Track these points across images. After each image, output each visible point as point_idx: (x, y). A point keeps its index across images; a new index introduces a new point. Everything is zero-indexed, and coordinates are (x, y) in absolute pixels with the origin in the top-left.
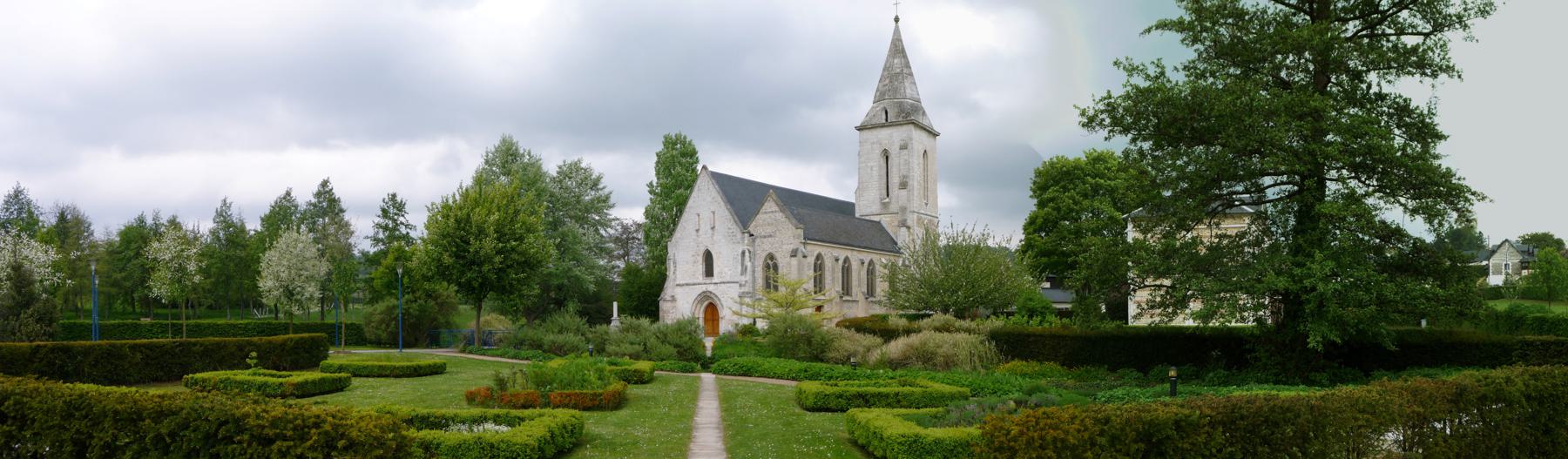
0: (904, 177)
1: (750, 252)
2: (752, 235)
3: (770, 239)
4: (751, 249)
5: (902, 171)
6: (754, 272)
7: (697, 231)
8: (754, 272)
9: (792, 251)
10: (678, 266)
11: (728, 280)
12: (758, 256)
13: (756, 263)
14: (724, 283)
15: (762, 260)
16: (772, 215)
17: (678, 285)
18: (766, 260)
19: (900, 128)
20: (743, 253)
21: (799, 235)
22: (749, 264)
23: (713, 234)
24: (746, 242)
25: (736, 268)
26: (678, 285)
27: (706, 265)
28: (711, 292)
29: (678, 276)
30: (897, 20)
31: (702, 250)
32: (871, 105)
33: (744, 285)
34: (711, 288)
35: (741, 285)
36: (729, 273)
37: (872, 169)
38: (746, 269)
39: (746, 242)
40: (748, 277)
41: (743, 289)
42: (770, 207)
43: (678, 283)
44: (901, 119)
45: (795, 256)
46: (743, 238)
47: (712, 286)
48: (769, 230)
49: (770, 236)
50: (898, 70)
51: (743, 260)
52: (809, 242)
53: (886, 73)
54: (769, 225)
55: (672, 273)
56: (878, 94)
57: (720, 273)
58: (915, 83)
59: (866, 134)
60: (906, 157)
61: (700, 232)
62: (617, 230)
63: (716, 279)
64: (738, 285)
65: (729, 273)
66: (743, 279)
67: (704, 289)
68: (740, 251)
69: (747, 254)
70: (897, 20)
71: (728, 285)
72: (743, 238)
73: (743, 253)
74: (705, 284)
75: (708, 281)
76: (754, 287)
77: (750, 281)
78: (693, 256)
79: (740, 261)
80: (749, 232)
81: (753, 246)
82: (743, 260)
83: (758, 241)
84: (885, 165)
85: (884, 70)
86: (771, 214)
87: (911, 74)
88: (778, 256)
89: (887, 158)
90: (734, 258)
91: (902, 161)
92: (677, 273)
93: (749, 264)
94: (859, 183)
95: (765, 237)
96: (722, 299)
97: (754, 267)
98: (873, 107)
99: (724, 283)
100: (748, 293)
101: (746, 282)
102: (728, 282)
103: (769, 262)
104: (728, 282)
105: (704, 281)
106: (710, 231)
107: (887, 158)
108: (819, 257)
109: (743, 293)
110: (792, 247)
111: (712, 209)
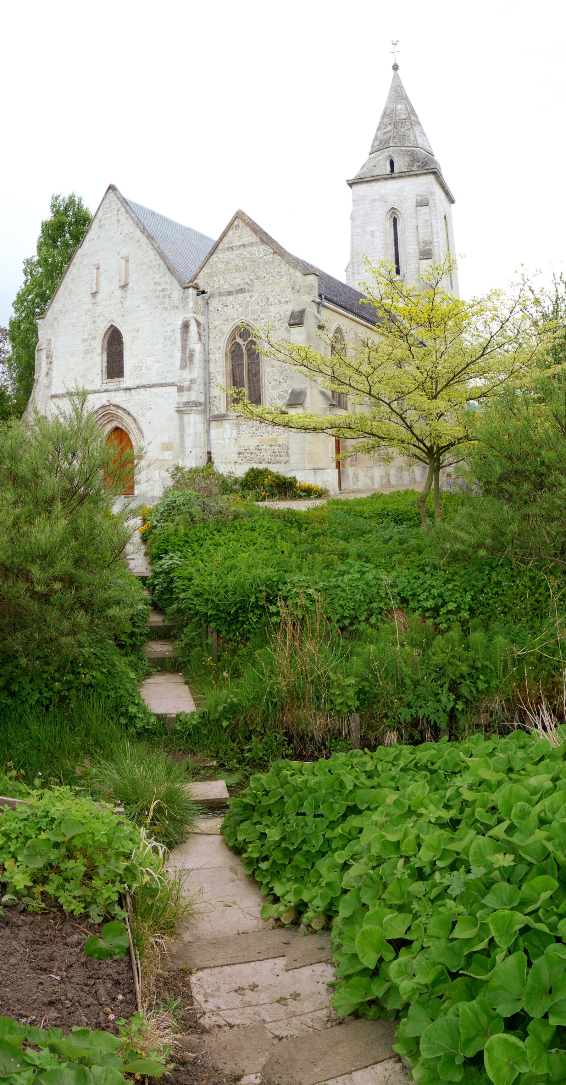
0: (425, 243)
1: (198, 324)
2: (203, 292)
3: (240, 297)
4: (202, 319)
5: (421, 236)
6: (207, 362)
7: (94, 294)
8: (207, 362)
9: (292, 315)
10: (55, 362)
11: (154, 381)
12: (214, 332)
13: (212, 345)
14: (144, 387)
15: (226, 337)
16: (245, 253)
17: (53, 397)
18: (232, 338)
19: (414, 180)
20: (186, 326)
21: (311, 287)
22: (197, 347)
23: (124, 298)
24: (191, 305)
25: (170, 357)
26: (53, 397)
27: (109, 356)
28: (117, 407)
29: (54, 380)
30: (395, 67)
31: (103, 327)
32: (366, 157)
33: (189, 389)
34: (118, 398)
35: (181, 389)
36: (156, 366)
37: (372, 236)
38: (192, 356)
39: (191, 305)
40: (196, 372)
41: (186, 397)
42: (240, 237)
43: (54, 393)
44: (415, 168)
45: (300, 324)
46: (185, 299)
47: (122, 393)
48: (238, 280)
49: (242, 291)
50: (404, 117)
51: (185, 339)
52: (326, 304)
53: (387, 120)
54: (238, 270)
55: (43, 375)
56: (377, 143)
57: (137, 368)
58: (424, 134)
59: (362, 189)
60: (427, 217)
61: (99, 297)
62: (542, 508)
63: (128, 380)
64: (175, 389)
65: (156, 366)
66: (186, 376)
67: (105, 402)
68: (179, 323)
69: (193, 327)
70: (395, 67)
71: (153, 389)
72: (185, 299)
73: (186, 326)
74: (106, 391)
75: (113, 384)
76: (207, 392)
77: (200, 381)
78: (84, 340)
79: (179, 343)
80: (196, 287)
81: (206, 313)
82: (185, 339)
83: (215, 302)
84: (392, 230)
85: (383, 117)
86: (241, 250)
87: (419, 123)
88: (259, 328)
89: (395, 221)
90: (167, 338)
91: (421, 222)
92: (54, 374)
93: (197, 347)
94: (352, 257)
95: (230, 293)
96: (139, 419)
97: (206, 352)
98: (370, 159)
99: (144, 387)
100: (196, 404)
101: (192, 381)
102: (153, 386)
103: (239, 340)
104: (153, 386)
105: (105, 387)
106: (119, 292)
107: (395, 221)
108: (338, 330)
109: (187, 404)
110: (289, 309)
111: (124, 252)
